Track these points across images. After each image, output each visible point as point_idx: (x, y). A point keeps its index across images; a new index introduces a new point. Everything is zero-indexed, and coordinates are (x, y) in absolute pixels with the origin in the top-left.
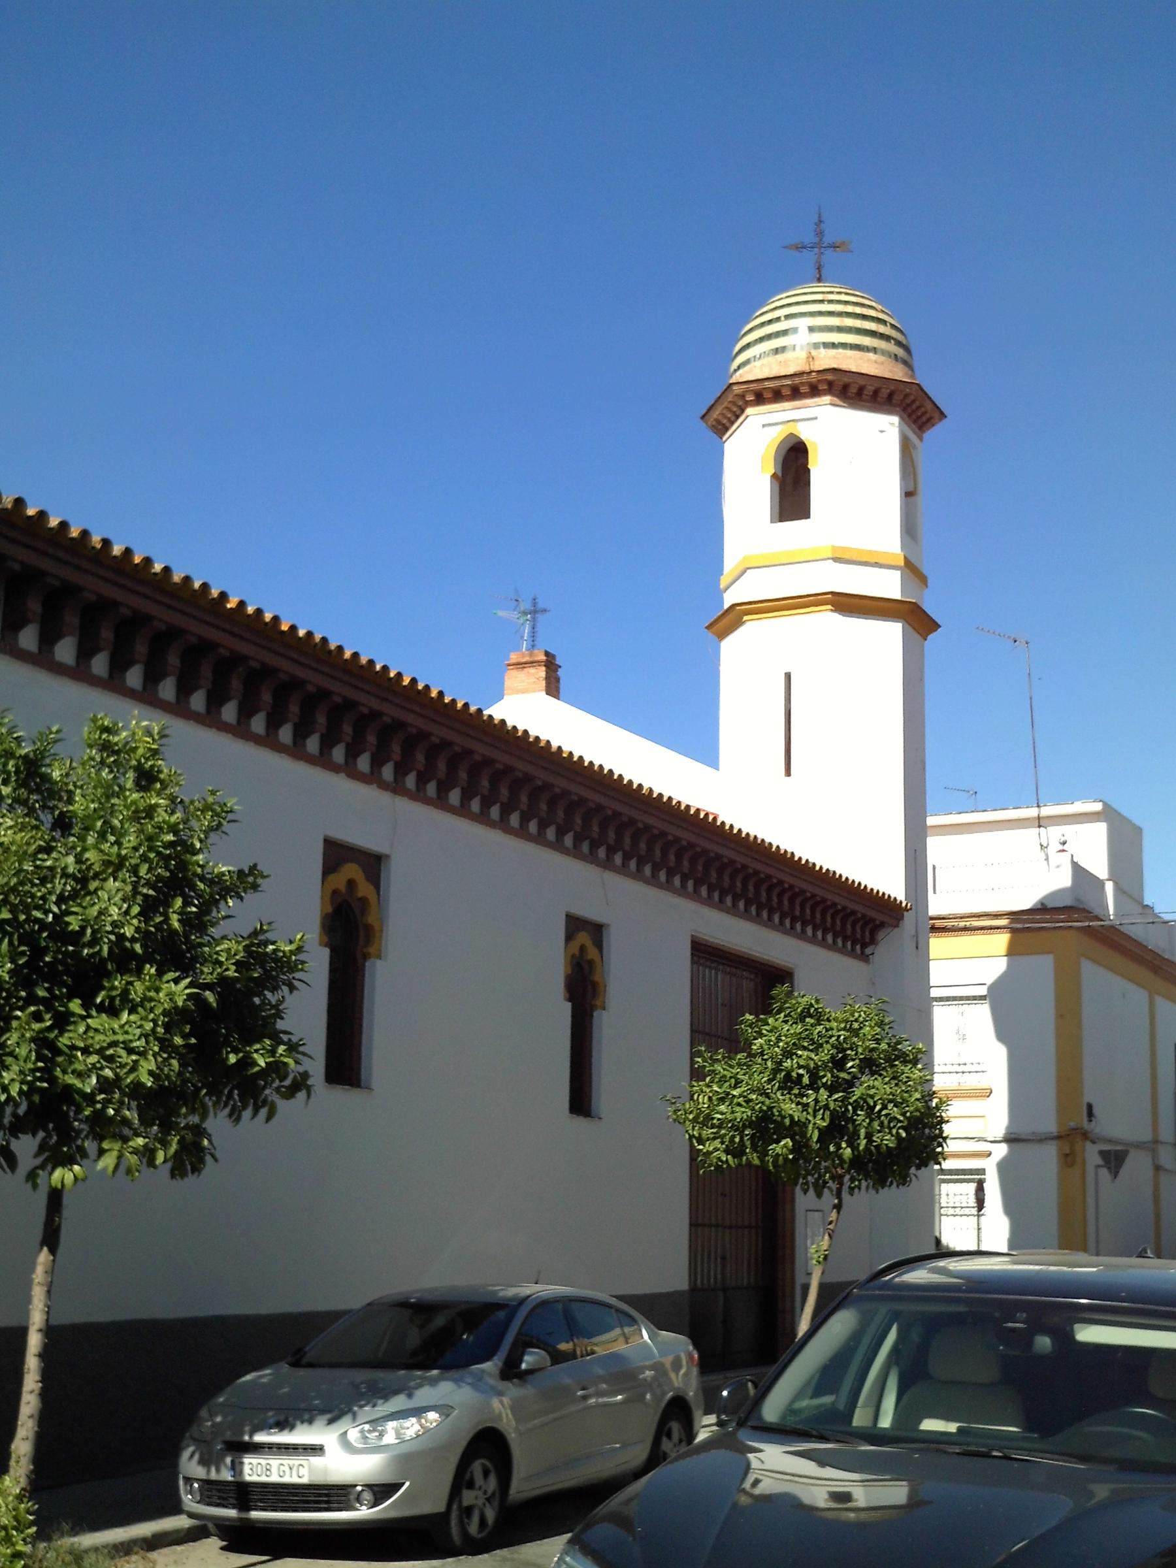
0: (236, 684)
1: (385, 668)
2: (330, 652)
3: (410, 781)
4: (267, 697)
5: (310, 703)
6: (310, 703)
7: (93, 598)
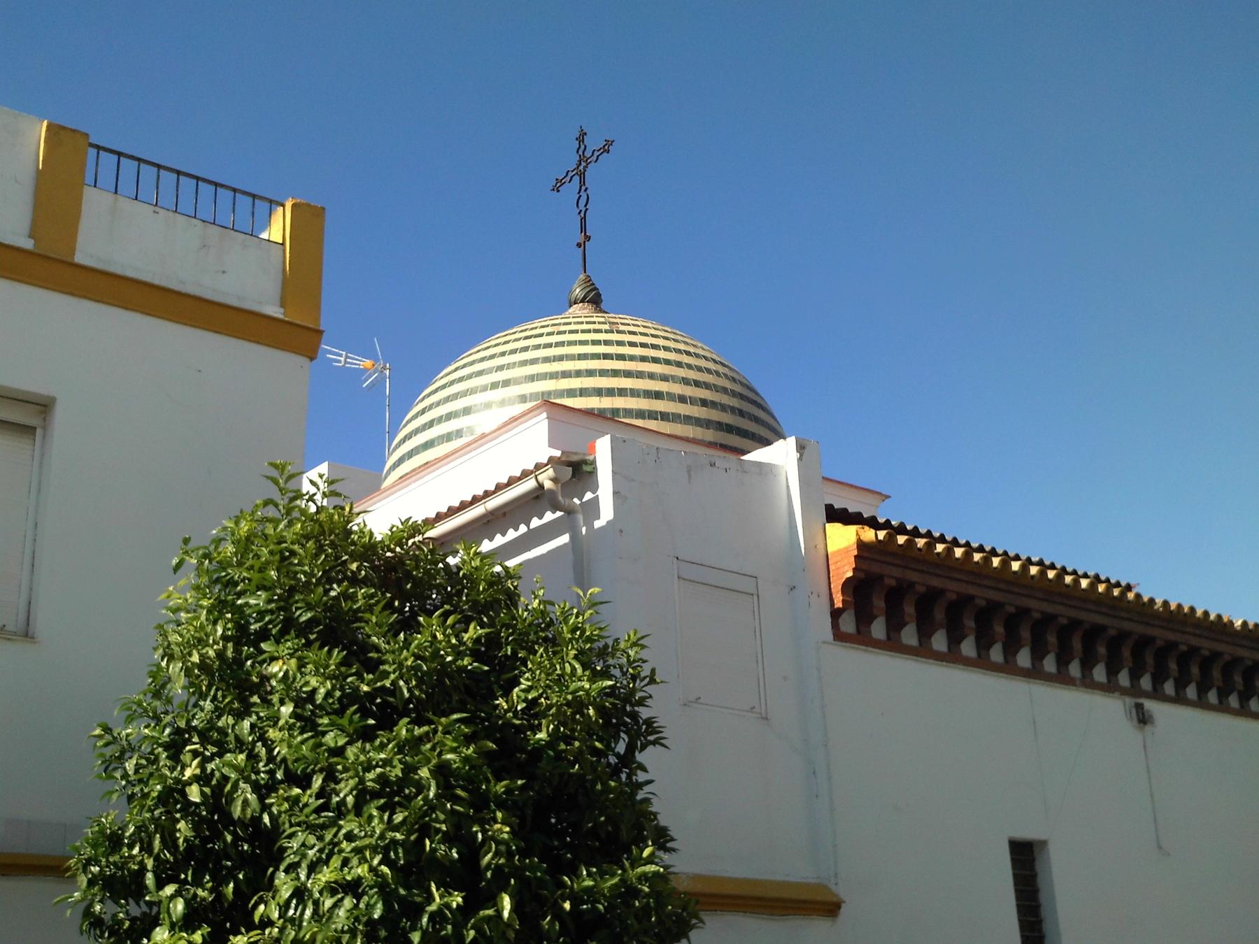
0: (1025, 634)
1: (1206, 613)
2: (1144, 604)
3: (1212, 697)
4: (999, 629)
5: (1064, 635)
6: (1064, 635)
7: (983, 603)
